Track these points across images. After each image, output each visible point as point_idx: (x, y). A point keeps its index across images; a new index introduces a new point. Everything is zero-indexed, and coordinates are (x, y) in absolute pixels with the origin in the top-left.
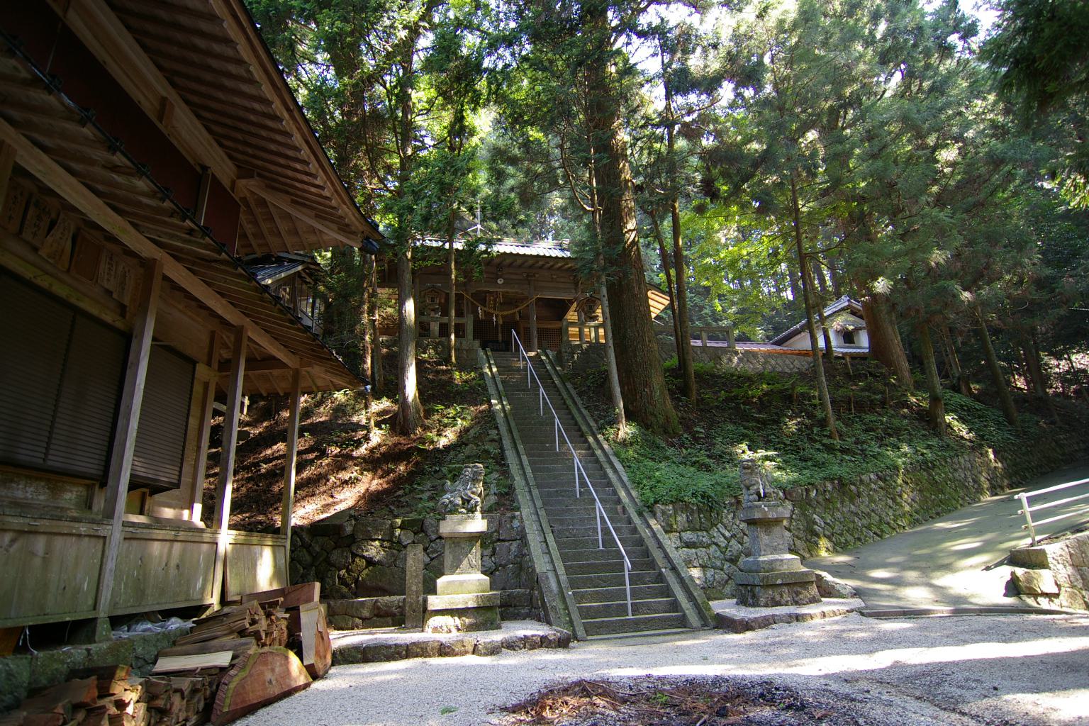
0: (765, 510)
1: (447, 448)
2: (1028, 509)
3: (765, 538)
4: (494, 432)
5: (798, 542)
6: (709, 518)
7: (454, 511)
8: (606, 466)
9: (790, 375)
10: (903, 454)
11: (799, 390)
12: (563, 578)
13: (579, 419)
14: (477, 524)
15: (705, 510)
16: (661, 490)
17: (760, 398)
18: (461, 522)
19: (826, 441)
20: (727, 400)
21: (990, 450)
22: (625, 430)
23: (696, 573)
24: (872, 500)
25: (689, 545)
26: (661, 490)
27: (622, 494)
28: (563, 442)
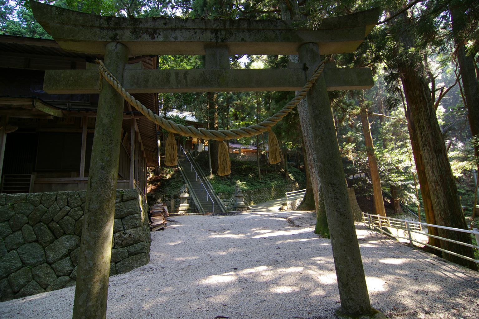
0: (239, 194)
1: (169, 179)
2: (287, 196)
3: (238, 199)
4: (181, 176)
5: (247, 202)
6: (229, 196)
7: (183, 193)
8: (208, 184)
9: (254, 162)
10: (274, 184)
11: (254, 167)
12: (201, 206)
13: (201, 173)
14: (187, 195)
15: (228, 194)
16: (220, 190)
17: (245, 169)
18: (184, 195)
19: (258, 180)
20: (237, 169)
21: (297, 183)
22: (212, 176)
23: (226, 206)
24: (265, 194)
25: (225, 201)
26: (220, 190)
27: (212, 191)
28: (198, 178)
